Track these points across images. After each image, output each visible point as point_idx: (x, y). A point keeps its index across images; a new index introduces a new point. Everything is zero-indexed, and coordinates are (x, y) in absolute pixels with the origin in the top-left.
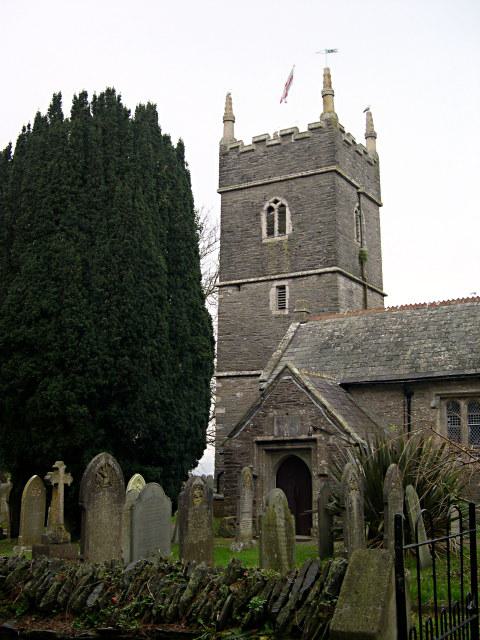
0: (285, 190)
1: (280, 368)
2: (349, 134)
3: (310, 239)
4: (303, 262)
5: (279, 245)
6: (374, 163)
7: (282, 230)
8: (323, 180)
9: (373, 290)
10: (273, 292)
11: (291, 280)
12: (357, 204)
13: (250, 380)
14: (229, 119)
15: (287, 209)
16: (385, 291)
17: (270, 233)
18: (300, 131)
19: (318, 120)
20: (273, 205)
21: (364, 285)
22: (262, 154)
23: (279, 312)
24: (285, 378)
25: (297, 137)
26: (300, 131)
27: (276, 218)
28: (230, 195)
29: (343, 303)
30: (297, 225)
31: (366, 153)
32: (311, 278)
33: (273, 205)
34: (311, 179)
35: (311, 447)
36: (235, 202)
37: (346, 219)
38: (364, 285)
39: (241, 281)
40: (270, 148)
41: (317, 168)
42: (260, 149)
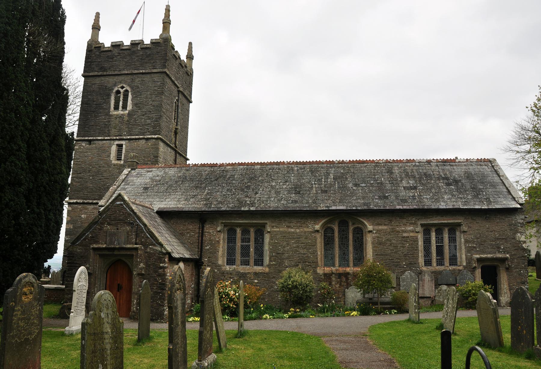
0: (129, 81)
1: (115, 195)
2: (177, 52)
3: (143, 115)
4: (137, 131)
5: (121, 117)
6: (189, 75)
7: (125, 107)
8: (156, 78)
9: (181, 155)
10: (114, 148)
11: (127, 141)
12: (177, 98)
13: (92, 206)
14: (96, 28)
15: (130, 94)
16: (188, 157)
17: (116, 108)
18: (145, 43)
19: (158, 38)
20: (120, 89)
21: (176, 151)
22: (117, 54)
23: (116, 162)
24: (118, 203)
25: (143, 46)
26: (145, 43)
27: (121, 99)
28: (90, 80)
29: (161, 160)
30: (135, 105)
31: (186, 67)
32: (141, 141)
33: (120, 89)
34: (148, 76)
35: (134, 254)
36: (94, 84)
37: (168, 108)
38: (176, 151)
39: (92, 138)
40: (124, 52)
41: (154, 69)
42: (116, 51)
